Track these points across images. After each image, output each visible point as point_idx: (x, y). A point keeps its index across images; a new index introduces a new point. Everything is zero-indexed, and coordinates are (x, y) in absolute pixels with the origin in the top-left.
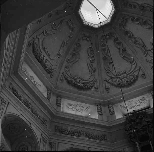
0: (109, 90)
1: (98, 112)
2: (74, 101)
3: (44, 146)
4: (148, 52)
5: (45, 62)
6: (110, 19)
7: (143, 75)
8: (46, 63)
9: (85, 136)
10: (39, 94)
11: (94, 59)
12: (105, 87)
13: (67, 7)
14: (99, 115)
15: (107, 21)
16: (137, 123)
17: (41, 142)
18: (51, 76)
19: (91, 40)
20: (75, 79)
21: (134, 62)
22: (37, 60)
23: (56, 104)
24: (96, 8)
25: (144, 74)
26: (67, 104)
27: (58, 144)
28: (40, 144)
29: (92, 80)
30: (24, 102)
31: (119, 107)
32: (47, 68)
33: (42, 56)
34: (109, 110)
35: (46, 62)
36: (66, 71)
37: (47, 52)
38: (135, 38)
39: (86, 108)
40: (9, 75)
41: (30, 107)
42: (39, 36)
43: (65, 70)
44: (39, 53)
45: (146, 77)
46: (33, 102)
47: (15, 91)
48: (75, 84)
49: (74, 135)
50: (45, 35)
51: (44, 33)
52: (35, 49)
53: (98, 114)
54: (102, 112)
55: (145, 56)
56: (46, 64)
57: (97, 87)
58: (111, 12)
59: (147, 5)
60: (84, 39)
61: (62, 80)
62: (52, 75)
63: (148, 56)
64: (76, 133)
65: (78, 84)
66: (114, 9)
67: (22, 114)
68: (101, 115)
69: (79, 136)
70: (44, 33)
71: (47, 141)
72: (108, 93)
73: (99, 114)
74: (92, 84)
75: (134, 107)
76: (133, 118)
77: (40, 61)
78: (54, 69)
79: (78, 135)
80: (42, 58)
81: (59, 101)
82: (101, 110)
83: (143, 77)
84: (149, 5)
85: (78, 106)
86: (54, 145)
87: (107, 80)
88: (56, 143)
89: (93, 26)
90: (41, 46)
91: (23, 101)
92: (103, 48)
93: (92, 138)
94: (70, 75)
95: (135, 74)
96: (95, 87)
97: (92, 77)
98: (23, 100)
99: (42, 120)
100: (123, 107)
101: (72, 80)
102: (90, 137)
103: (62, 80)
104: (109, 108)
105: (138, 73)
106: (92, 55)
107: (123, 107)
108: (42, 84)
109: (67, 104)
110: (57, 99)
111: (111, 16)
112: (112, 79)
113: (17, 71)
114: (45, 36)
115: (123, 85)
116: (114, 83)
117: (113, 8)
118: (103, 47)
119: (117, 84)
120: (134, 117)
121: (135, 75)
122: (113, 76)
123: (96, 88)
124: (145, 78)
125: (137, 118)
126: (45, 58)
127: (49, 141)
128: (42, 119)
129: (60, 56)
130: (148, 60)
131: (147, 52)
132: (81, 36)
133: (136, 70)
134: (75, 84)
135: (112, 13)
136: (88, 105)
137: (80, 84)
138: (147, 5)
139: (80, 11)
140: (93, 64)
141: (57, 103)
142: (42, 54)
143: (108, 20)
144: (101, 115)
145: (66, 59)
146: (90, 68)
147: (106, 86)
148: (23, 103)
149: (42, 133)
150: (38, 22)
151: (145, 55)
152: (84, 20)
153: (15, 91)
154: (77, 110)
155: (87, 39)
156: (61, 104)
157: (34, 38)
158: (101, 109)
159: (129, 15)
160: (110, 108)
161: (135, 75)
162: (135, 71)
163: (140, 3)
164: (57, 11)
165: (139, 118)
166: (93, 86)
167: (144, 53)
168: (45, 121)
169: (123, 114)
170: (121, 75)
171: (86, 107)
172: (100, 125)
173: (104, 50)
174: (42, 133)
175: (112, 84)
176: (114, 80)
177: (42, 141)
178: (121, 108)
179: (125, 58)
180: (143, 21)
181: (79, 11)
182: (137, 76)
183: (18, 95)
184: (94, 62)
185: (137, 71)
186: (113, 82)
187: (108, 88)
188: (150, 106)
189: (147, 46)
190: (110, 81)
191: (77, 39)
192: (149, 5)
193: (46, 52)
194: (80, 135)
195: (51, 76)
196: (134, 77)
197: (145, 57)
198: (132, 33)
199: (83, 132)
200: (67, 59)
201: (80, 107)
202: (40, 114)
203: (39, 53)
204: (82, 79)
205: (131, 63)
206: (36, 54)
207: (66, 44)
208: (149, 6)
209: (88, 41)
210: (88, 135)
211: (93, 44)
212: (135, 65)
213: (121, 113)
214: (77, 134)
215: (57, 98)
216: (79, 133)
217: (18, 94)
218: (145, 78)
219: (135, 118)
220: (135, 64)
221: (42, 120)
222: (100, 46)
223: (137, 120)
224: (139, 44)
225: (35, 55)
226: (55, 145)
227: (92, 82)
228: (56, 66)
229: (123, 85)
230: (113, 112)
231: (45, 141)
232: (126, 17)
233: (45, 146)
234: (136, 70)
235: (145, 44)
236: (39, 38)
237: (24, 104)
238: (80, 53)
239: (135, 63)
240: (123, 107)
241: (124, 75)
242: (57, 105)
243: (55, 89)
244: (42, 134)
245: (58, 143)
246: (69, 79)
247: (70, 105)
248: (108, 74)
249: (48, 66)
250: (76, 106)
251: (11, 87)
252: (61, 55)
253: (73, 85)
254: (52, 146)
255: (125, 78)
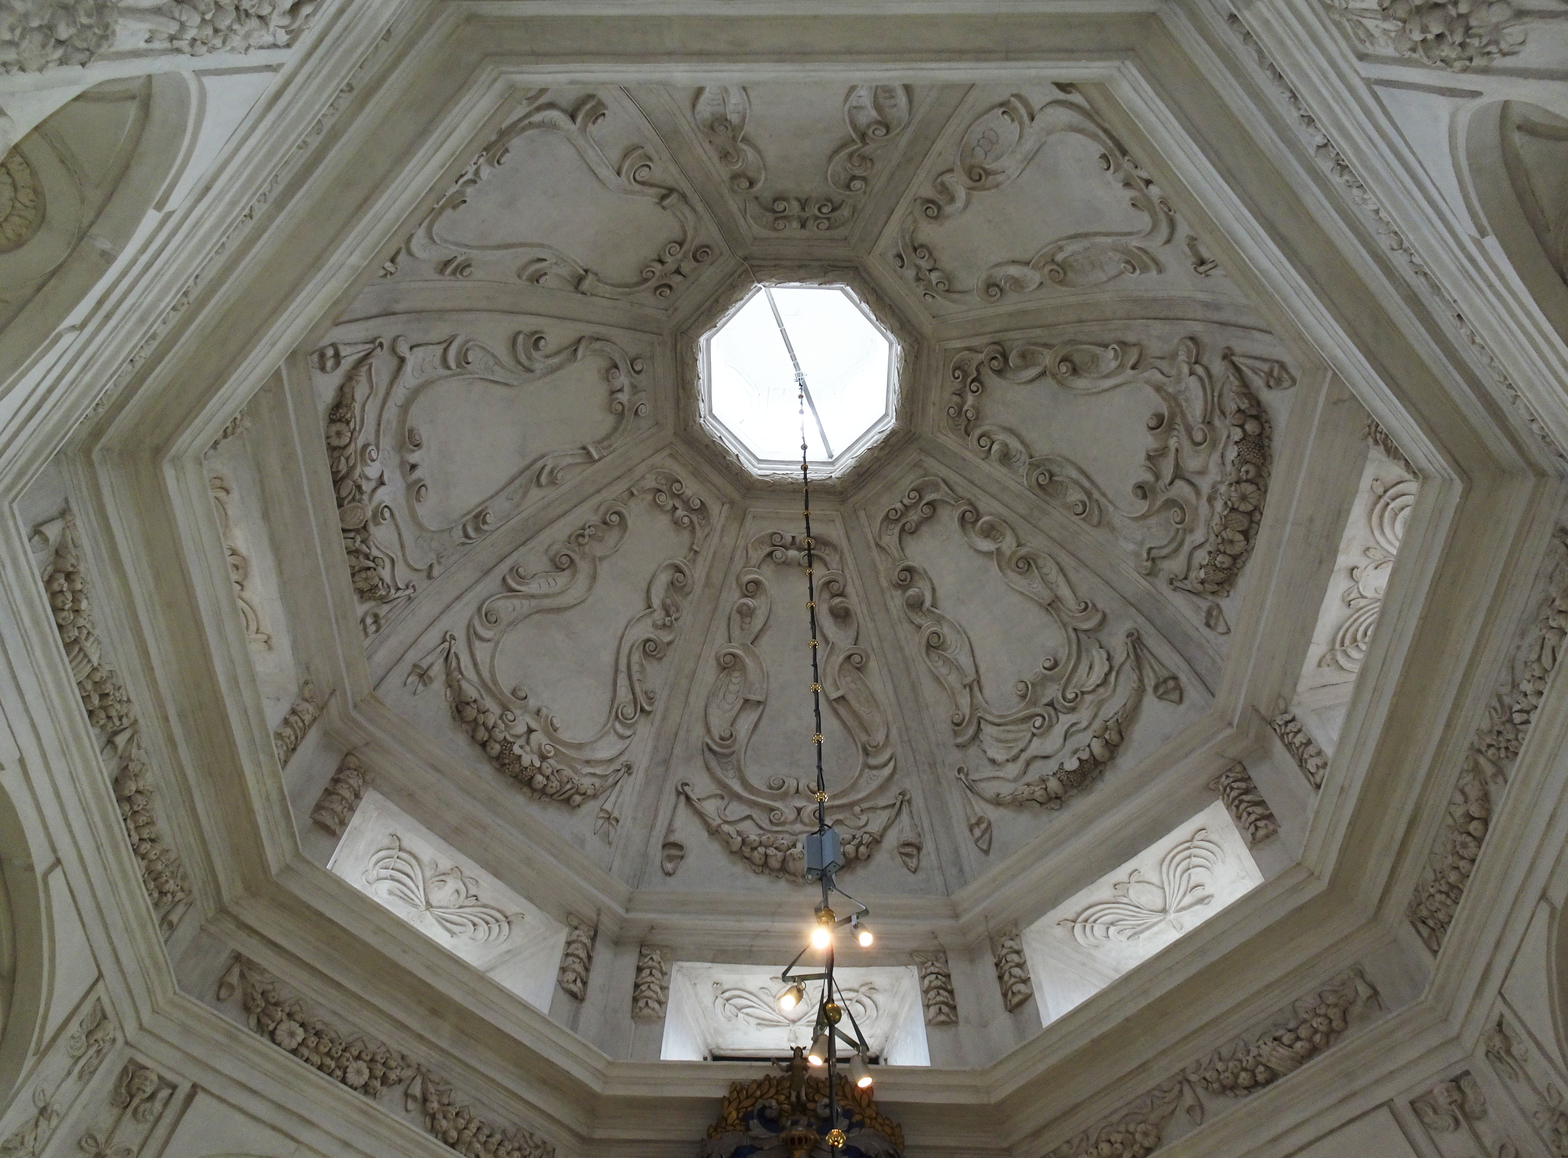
0: (682, 857)
1: (563, 970)
2: (445, 838)
3: (69, 1073)
4: (983, 725)
5: (369, 514)
6: (847, 463)
7: (909, 850)
8: (377, 524)
9: (411, 1105)
10: (234, 681)
11: (670, 643)
12: (664, 832)
13: (646, 280)
14: (561, 992)
15: (831, 468)
16: (792, 1140)
17: (61, 1042)
18: (369, 621)
19: (697, 526)
20: (505, 708)
21: (886, 756)
22: (335, 473)
23: (319, 808)
24: (796, 366)
25: (919, 849)
26: (386, 842)
27: (190, 1099)
28: (42, 1054)
29: (611, 761)
30: (89, 686)
31: (706, 992)
32: (367, 557)
33: (373, 471)
34: (637, 986)
35: (378, 515)
36: (472, 635)
37: (413, 467)
38: (940, 619)
39: (499, 916)
40: (87, 451)
41: (121, 740)
42: (411, 348)
43: (471, 620)
44: (360, 442)
45: (923, 863)
46: (166, 719)
47: (69, 576)
48: (490, 737)
49: (339, 1073)
50: (453, 365)
51: (446, 350)
52: (349, 407)
53: (560, 982)
54: (585, 983)
55: (958, 746)
56: (372, 528)
57: (616, 814)
58: (869, 431)
59: (1074, 474)
60: (659, 506)
61: (423, 676)
62: (376, 617)
63: (973, 750)
64: (358, 1058)
65: (513, 743)
66: (894, 421)
67: (22, 761)
68: (577, 998)
69: (366, 1089)
70: (446, 350)
71: (114, 1040)
72: (668, 874)
73: (563, 988)
74: (597, 782)
75: (794, 1022)
76: (774, 1103)
77: (344, 494)
78: (407, 587)
79: (366, 1085)
80: (367, 487)
81: (343, 798)
82: (587, 970)
83: (908, 860)
84: (1088, 477)
85: (452, 884)
86: (152, 1097)
87: (693, 797)
88: (174, 1087)
89: (742, 458)
90: (391, 412)
91: (88, 676)
92: (744, 600)
93: (454, 1134)
94: (486, 674)
95: (866, 825)
96: (608, 807)
97: (613, 738)
98: (95, 669)
99: (160, 874)
100: (727, 995)
101: (489, 703)
102: (444, 1123)
103: (423, 676)
104: (639, 970)
105: (886, 829)
106: (668, 614)
107: (728, 1000)
108: (283, 642)
109: (386, 842)
110: (336, 781)
111: (861, 450)
112: (722, 798)
113: (158, 452)
114: (448, 368)
115: (774, 863)
116: (726, 828)
117: (886, 415)
118: (746, 596)
119: (744, 842)
120: (783, 1098)
121: (868, 829)
122: (737, 787)
123: (610, 818)
124: (914, 872)
125: (800, 1107)
126: (383, 495)
127: (129, 1052)
128: (159, 867)
129: (477, 529)
130: (967, 775)
131: (979, 729)
132: (650, 482)
133: (882, 802)
134: (490, 737)
135: (875, 438)
136: (514, 903)
137: (521, 747)
138: (1074, 474)
139: (708, 341)
140: (652, 668)
141: (326, 804)
142: (373, 460)
143: (832, 464)
144: (573, 995)
145: (504, 567)
146: (622, 680)
147: (670, 830)
148: (79, 684)
149: (108, 967)
150: (447, 263)
151: (959, 740)
152: (706, 400)
153: (69, 576)
154: (429, 905)
155: (680, 513)
156: (343, 823)
157: (372, 342)
158: (590, 957)
159: (956, 487)
160: (651, 974)
161: (868, 829)
162: (873, 809)
163: (1042, 448)
164: (586, 271)
165: (814, 1110)
166: (595, 796)
167: (958, 725)
168: (180, 895)
169: (707, 1045)
170: (784, 797)
171: (499, 911)
172: (547, 1061)
173: (746, 613)
174: (108, 967)
175: (714, 832)
176: (736, 810)
177: (74, 1028)
178: (708, 1000)
179: (842, 711)
180: (1023, 551)
181: (702, 340)
182: (876, 841)
183: (77, 611)
184: (660, 659)
185: (885, 808)
186: (726, 822)
187: (678, 846)
188: (882, 1051)
189: (989, 691)
190: (710, 807)
191: (620, 487)
192: (1088, 477)
193: (403, 462)
194: (377, 1084)
195: (369, 621)
196: (856, 842)
197: (957, 754)
198: (934, 590)
199: (408, 1073)
200: (511, 570)
201: (457, 891)
202: (163, 826)
203: (360, 442)
204: (551, 729)
205: (865, 750)
206: (339, 434)
207: (543, 479)
208: (1087, 484)
209: (676, 523)
210: (435, 1105)
211: (696, 552)
212: (887, 771)
213: (699, 1040)
214: (359, 1072)
215: (340, 770)
216: (379, 1071)
217: (84, 605)
218: (914, 872)
219: (786, 1107)
220: (885, 765)
221: (160, 874)
222: (732, 580)
223: (795, 1123)
224: (954, 665)
225: (335, 442)
226: (165, 1093)
227: (599, 771)
228: (430, 577)
229: (774, 863)
230: (656, 1006)
231: (99, 1035)
232: (937, 488)
233: (80, 1076)
234: (882, 802)
235: (983, 680)
236: (402, 360)
237: (86, 699)
238: (604, 569)
239: (891, 759)
240: (728, 1000)
241: (799, 804)
242: (319, 817)
243: (354, 714)
244: (100, 976)
245: (195, 1086)
246: (471, 692)
247: (403, 855)
248: (713, 764)
249: (375, 552)
250: (442, 877)
251: (53, 532)
252: (485, 527)
253: (482, 734)
254: (136, 1101)
255: (805, 825)
